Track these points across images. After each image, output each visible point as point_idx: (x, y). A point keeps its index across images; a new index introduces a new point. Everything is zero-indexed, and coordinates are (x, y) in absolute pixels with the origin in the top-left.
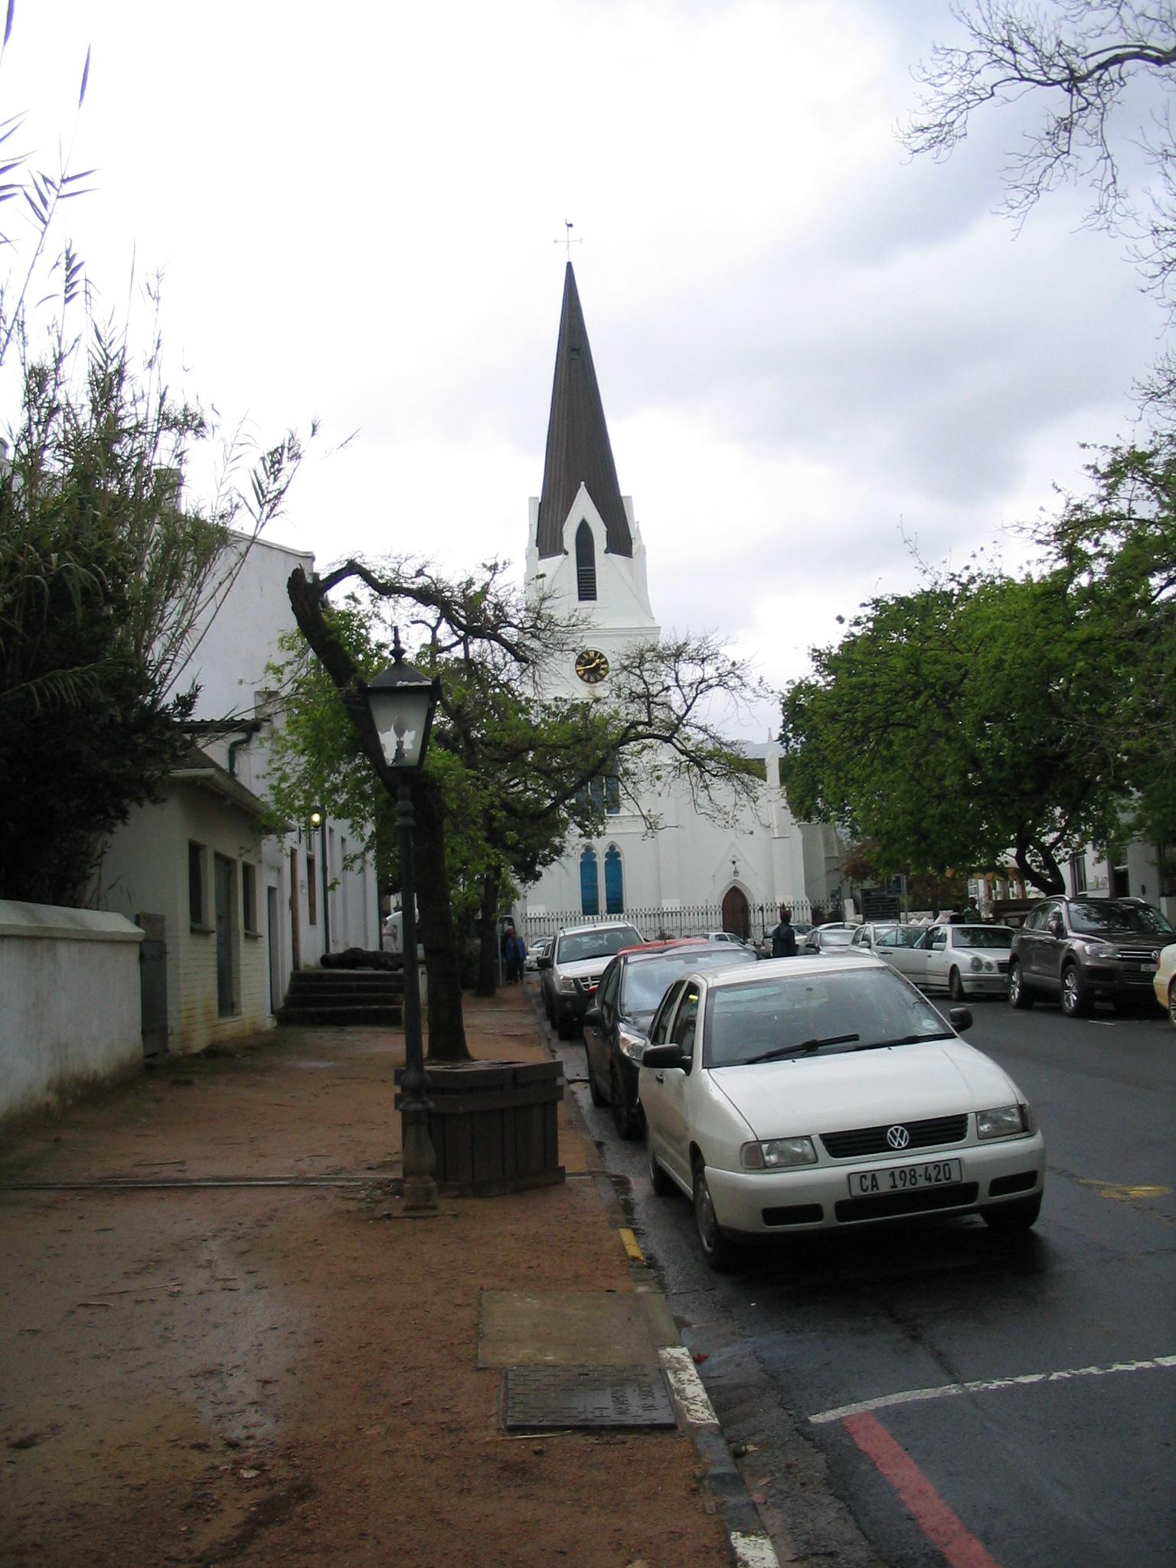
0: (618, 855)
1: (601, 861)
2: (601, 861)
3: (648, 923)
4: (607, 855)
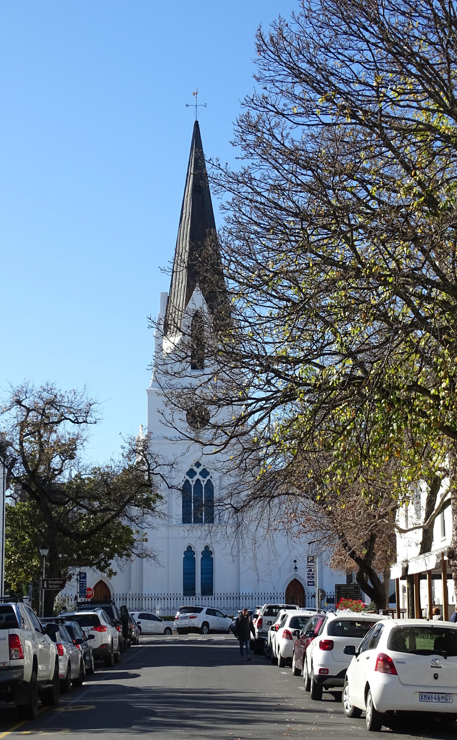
0: (211, 553)
1: (198, 557)
2: (198, 557)
3: (222, 603)
4: (203, 553)
